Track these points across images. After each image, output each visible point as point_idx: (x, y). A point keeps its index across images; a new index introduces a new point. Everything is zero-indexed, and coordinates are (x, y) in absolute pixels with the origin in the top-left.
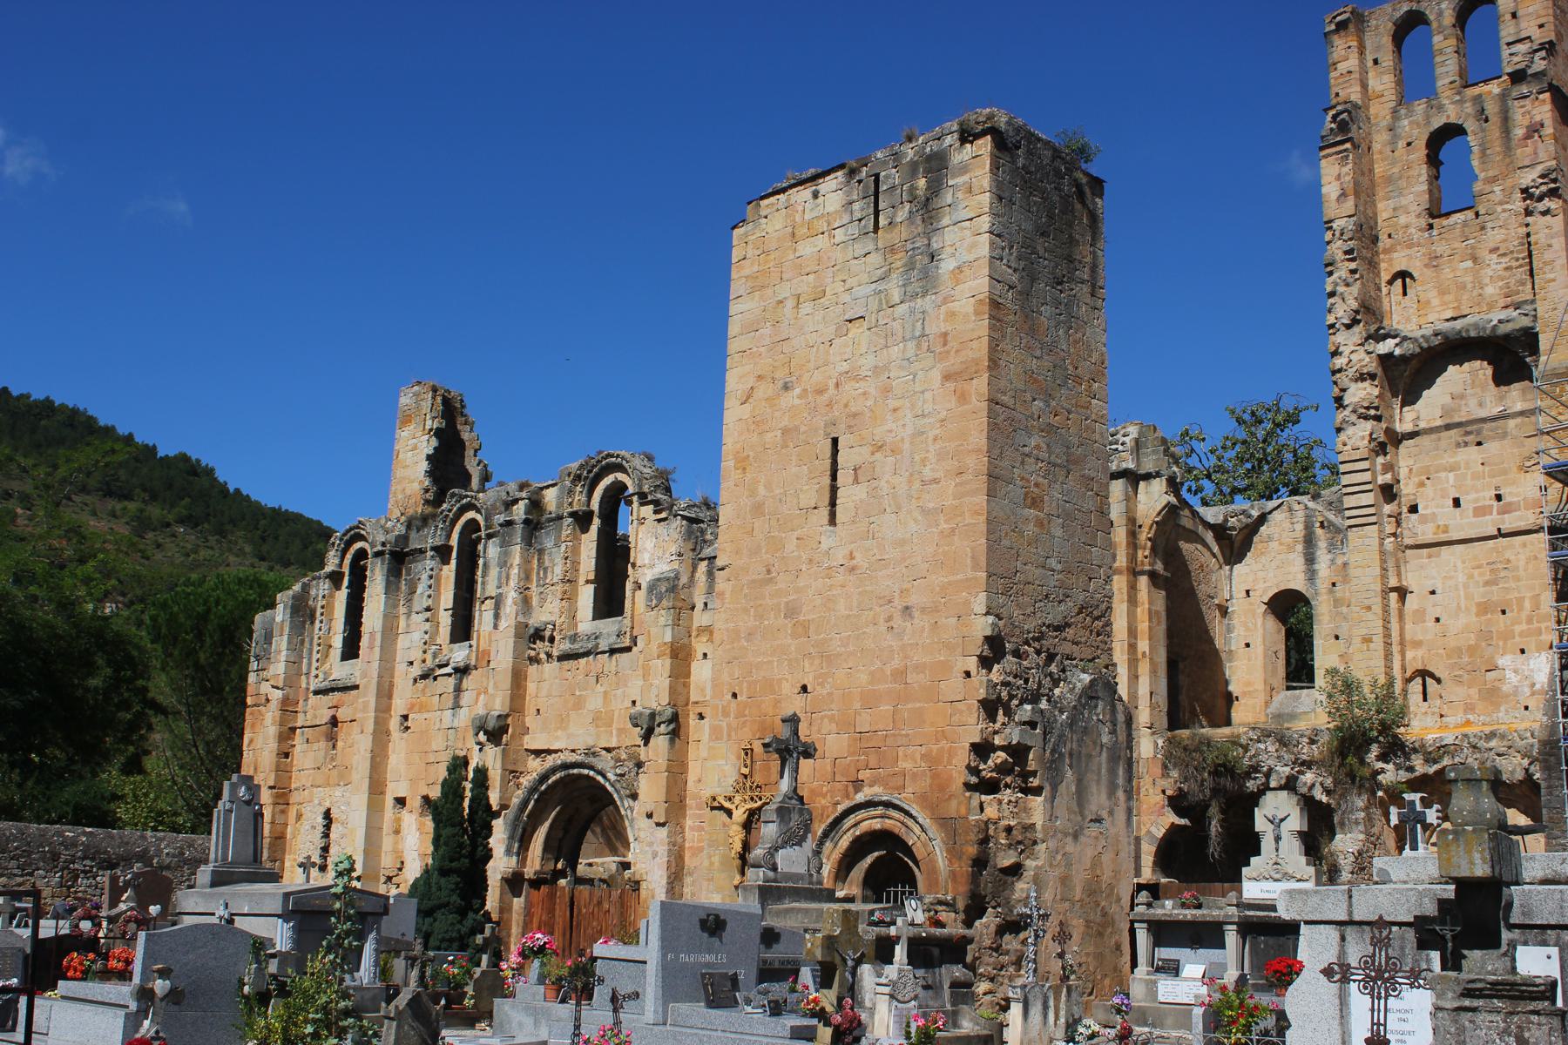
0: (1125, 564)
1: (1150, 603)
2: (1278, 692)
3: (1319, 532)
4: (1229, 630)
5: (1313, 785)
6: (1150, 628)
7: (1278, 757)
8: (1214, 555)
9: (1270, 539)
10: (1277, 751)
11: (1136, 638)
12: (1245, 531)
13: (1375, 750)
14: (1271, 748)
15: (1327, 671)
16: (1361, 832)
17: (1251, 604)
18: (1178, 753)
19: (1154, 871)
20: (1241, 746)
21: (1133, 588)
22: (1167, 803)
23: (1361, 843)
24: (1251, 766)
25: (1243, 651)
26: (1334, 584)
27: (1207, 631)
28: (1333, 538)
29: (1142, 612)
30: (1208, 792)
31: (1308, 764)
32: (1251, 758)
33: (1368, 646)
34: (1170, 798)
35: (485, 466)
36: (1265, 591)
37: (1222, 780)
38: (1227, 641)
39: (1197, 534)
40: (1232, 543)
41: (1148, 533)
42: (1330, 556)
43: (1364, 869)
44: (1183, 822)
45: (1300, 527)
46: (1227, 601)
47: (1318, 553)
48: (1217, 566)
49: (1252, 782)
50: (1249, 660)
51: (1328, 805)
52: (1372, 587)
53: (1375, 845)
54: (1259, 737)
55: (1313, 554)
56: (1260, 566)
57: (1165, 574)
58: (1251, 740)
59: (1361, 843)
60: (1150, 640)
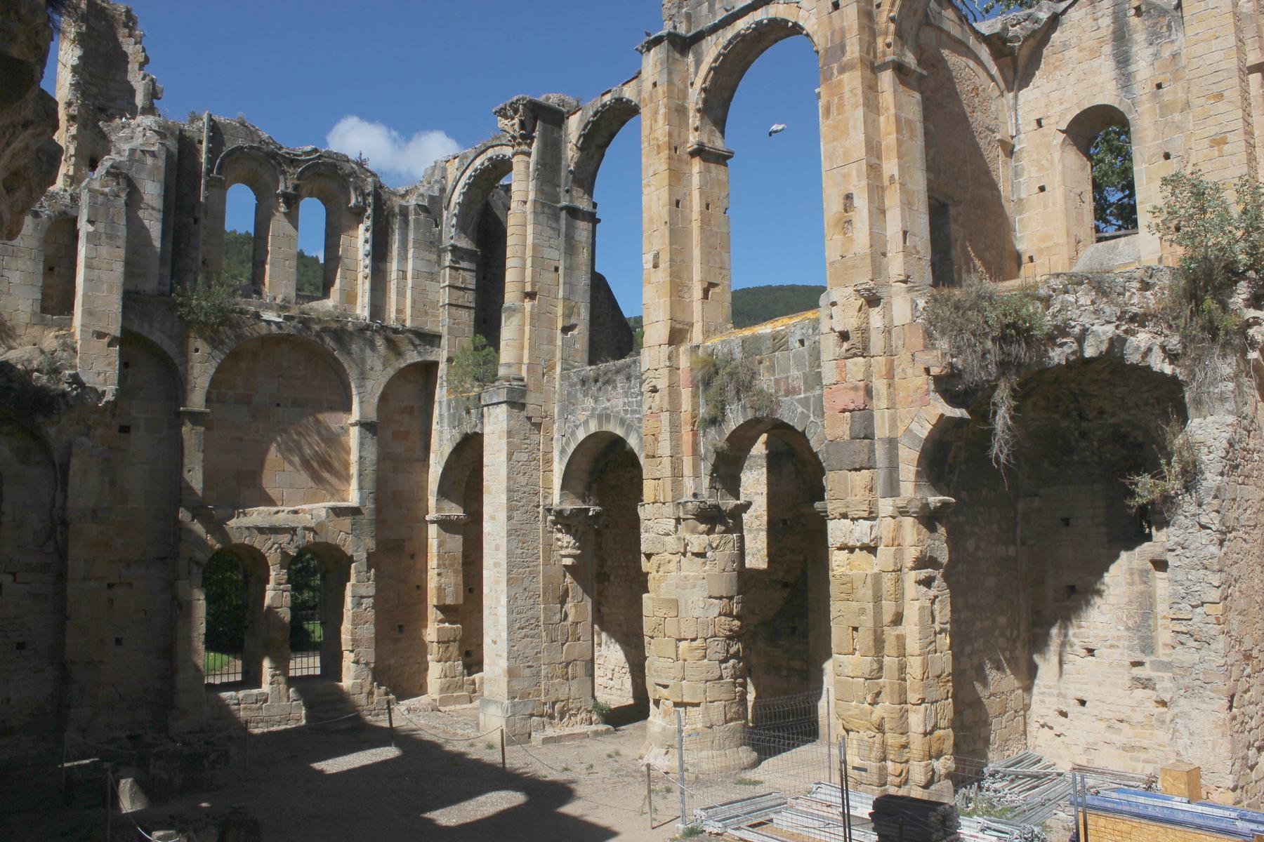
0: (857, 55)
1: (898, 106)
2: (1085, 246)
3: (1134, 21)
4: (1017, 174)
5: (1150, 349)
6: (900, 143)
7: (1096, 312)
8: (992, 78)
9: (1066, 46)
10: (1093, 303)
11: (879, 157)
12: (1031, 42)
13: (1242, 292)
14: (1085, 300)
15: (1164, 179)
16: (1230, 412)
17: (1044, 136)
18: (945, 312)
19: (917, 486)
20: (1039, 299)
21: (871, 89)
22: (932, 387)
23: (1230, 429)
24: (1056, 327)
25: (1036, 197)
26: (1159, 86)
27: (987, 172)
28: (1156, 24)
29: (886, 122)
30: (993, 369)
31: (1140, 320)
32: (1054, 316)
33: (1220, 151)
34: (937, 379)
35: (152, 80)
36: (1062, 115)
37: (1014, 349)
38: (1015, 188)
39: (968, 47)
40: (1015, 60)
41: (891, 11)
42: (1151, 50)
43: (1237, 467)
44: (959, 413)
45: (1106, 23)
46: (1012, 137)
47: (1135, 49)
48: (997, 93)
49: (1058, 350)
50: (1045, 207)
51: (1174, 377)
52: (1224, 65)
53: (1249, 432)
54: (1065, 286)
55: (1126, 52)
56: (1054, 85)
57: (919, 70)
58: (1054, 290)
59: (1230, 429)
60: (899, 158)
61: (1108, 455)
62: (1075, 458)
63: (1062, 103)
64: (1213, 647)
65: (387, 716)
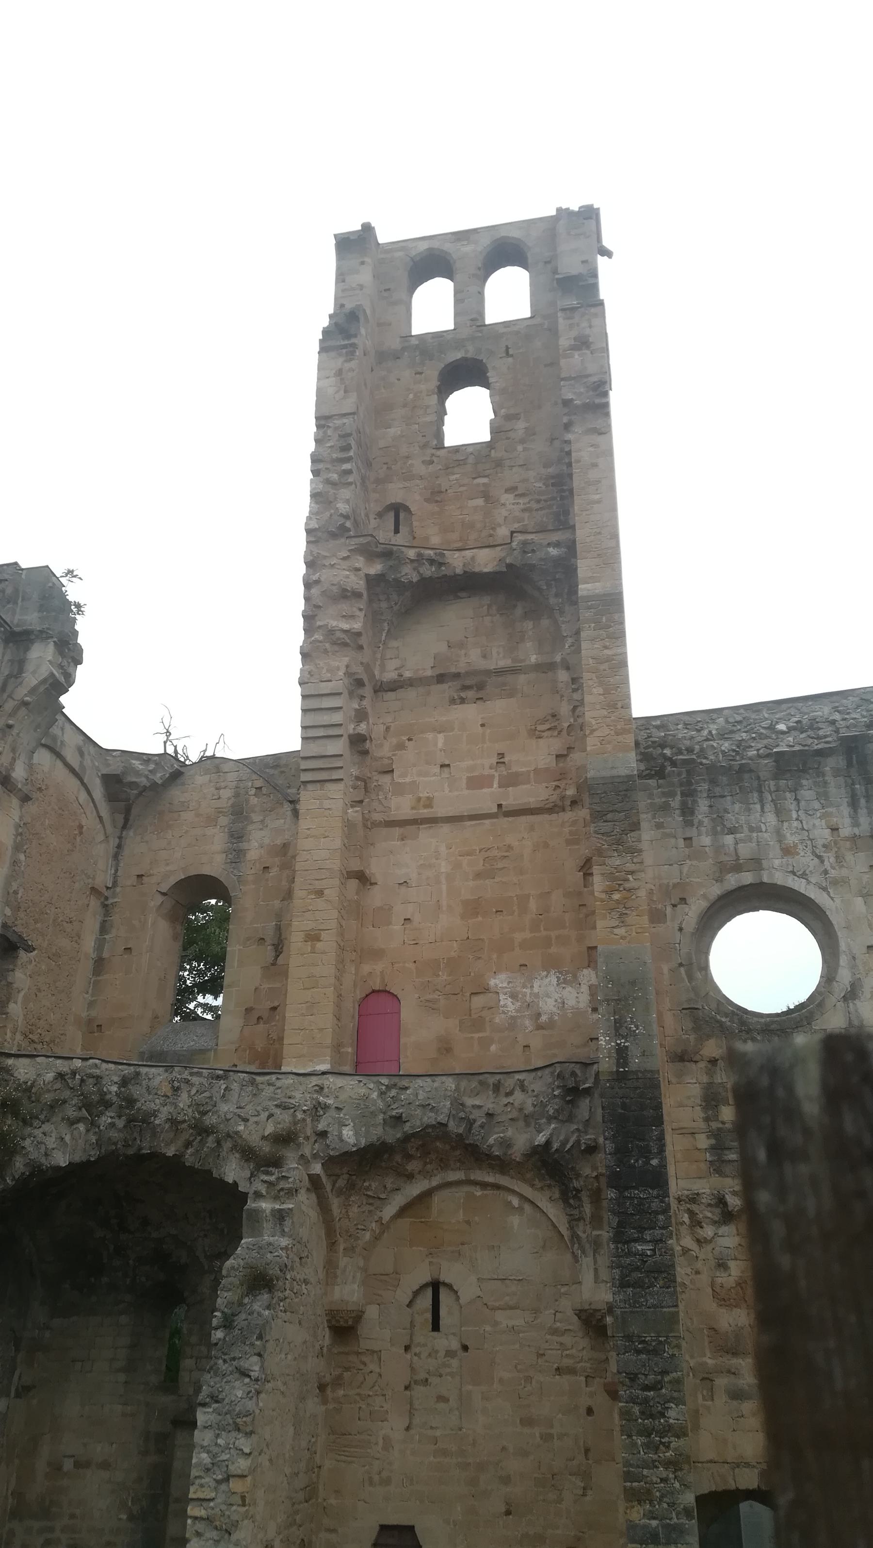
33: (313, 947)
61: (143, 1279)
62: (105, 1280)
63: (167, 864)
64: (234, 1537)
65: (671, 1304)
